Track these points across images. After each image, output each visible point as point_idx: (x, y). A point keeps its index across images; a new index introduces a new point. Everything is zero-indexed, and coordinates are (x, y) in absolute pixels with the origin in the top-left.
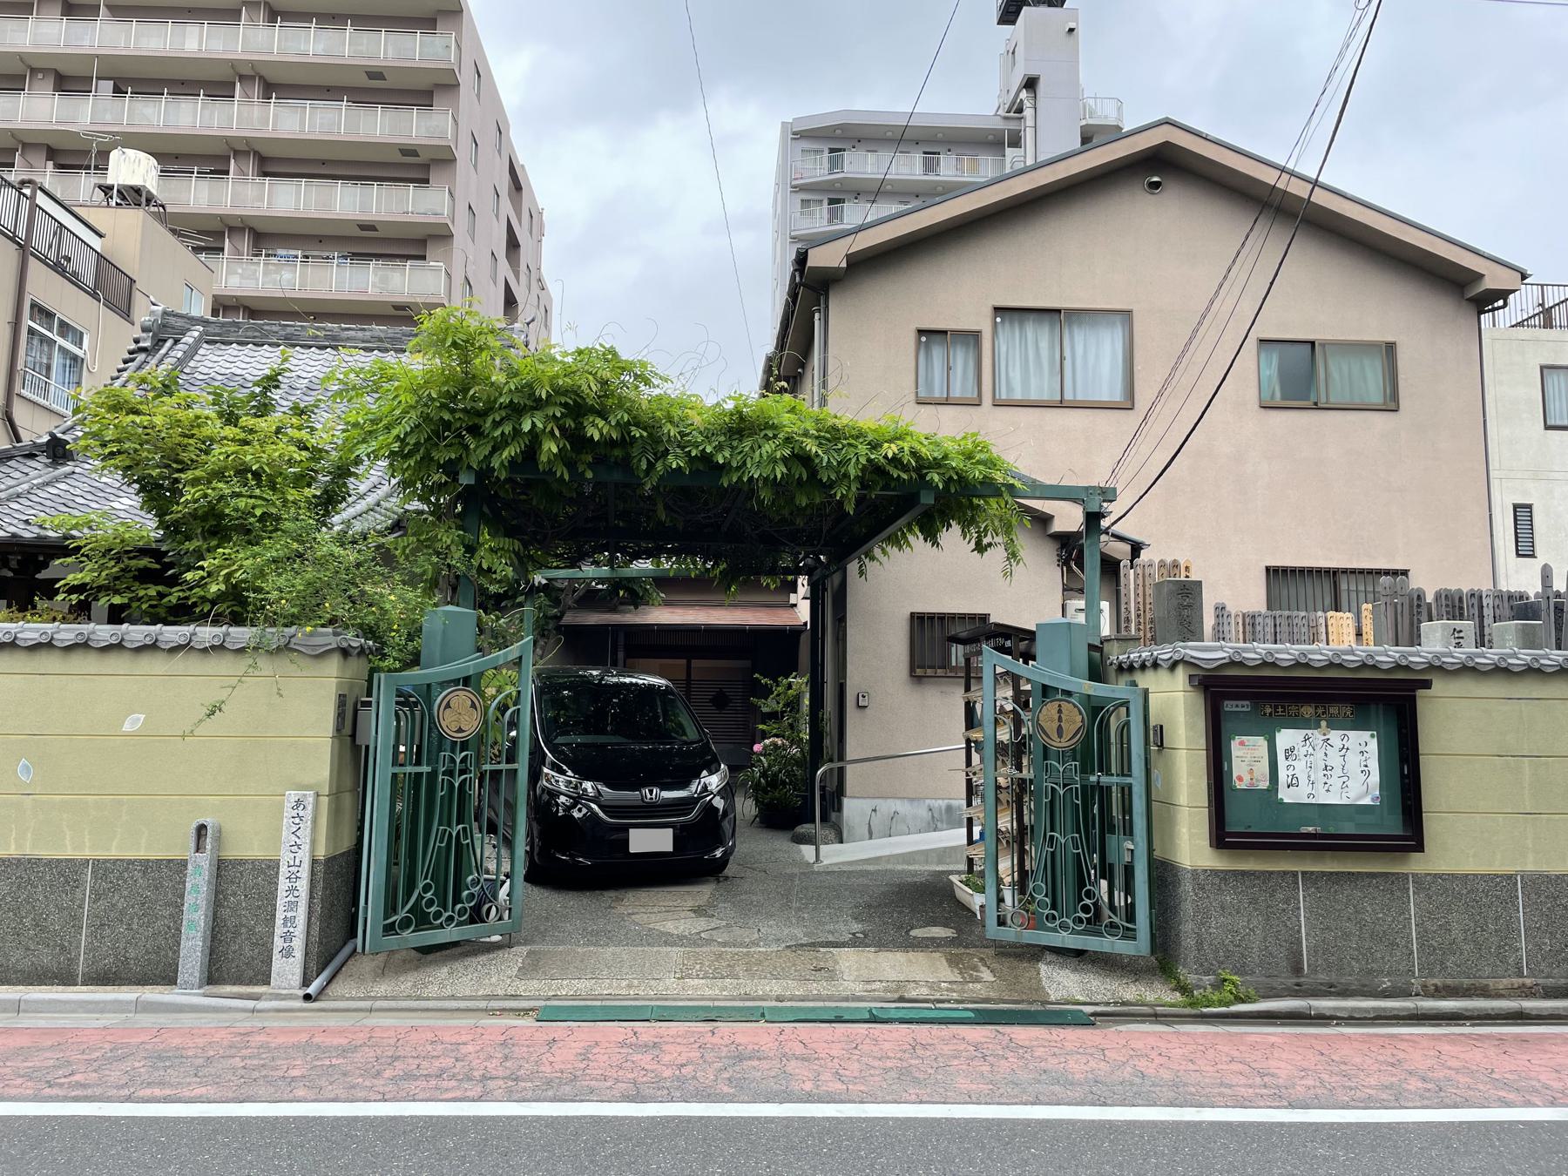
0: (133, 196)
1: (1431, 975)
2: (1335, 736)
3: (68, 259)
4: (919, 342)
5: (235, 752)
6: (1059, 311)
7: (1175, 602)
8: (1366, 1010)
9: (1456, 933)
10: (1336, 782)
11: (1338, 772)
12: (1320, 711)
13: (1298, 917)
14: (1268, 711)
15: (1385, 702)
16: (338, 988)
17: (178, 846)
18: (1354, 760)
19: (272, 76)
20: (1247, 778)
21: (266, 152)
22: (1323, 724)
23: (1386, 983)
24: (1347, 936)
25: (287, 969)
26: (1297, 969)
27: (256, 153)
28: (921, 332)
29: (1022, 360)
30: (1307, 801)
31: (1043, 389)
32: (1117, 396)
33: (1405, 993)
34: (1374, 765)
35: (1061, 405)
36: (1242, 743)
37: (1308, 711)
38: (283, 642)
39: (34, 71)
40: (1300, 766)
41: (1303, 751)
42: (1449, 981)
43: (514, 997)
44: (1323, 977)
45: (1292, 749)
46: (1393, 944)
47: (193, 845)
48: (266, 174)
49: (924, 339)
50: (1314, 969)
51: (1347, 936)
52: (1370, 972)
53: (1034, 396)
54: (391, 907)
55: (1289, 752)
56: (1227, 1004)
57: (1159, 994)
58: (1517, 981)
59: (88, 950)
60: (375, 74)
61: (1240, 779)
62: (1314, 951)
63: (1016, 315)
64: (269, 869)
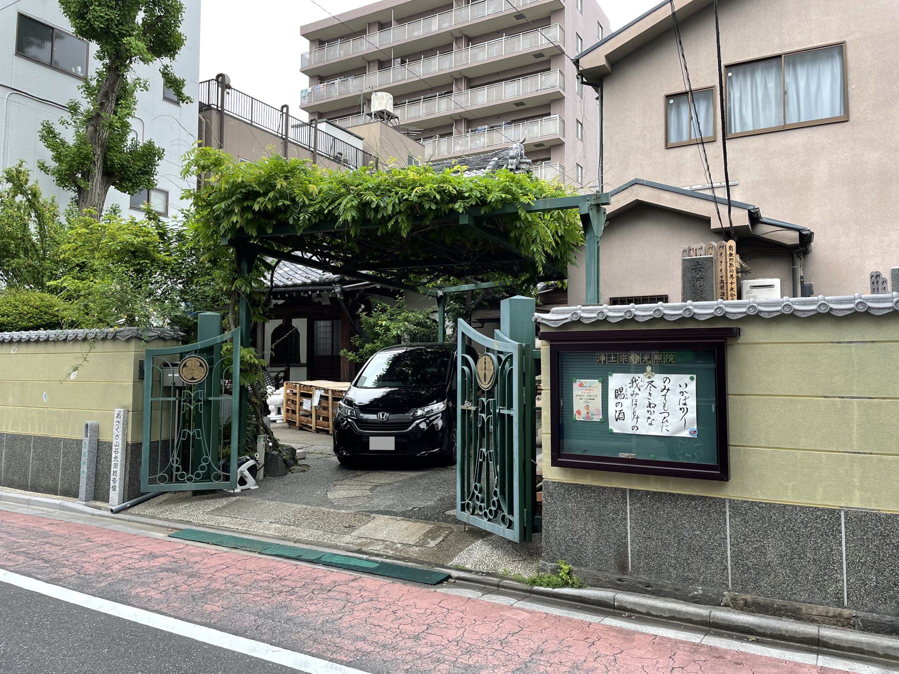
0: (383, 115)
1: (744, 590)
2: (658, 379)
3: (341, 154)
4: (667, 106)
5: (82, 390)
6: (780, 56)
7: (690, 276)
8: (661, 610)
9: (771, 556)
10: (657, 417)
11: (660, 408)
12: (646, 358)
13: (625, 526)
14: (603, 358)
15: (702, 349)
16: (135, 510)
17: (77, 433)
18: (674, 399)
19: (471, 34)
20: (584, 412)
21: (470, 76)
22: (649, 369)
23: (699, 590)
24: (666, 546)
25: (115, 496)
26: (623, 568)
27: (465, 77)
28: (668, 97)
29: (751, 102)
30: (631, 432)
31: (770, 119)
32: (838, 113)
33: (715, 603)
34: (692, 403)
35: (785, 129)
36: (581, 385)
37: (634, 358)
38: (104, 336)
39: (369, 62)
40: (627, 403)
41: (630, 391)
42: (761, 599)
43: (188, 522)
44: (644, 577)
45: (621, 390)
46: (708, 558)
47: (84, 433)
48: (471, 88)
49: (671, 101)
50: (637, 570)
51: (666, 546)
52: (686, 579)
53: (762, 126)
54: (153, 471)
55: (619, 392)
56: (555, 586)
57: (520, 570)
58: (833, 610)
59: (62, 479)
60: (519, 16)
61: (579, 412)
62: (638, 555)
63: (748, 66)
64: (110, 445)
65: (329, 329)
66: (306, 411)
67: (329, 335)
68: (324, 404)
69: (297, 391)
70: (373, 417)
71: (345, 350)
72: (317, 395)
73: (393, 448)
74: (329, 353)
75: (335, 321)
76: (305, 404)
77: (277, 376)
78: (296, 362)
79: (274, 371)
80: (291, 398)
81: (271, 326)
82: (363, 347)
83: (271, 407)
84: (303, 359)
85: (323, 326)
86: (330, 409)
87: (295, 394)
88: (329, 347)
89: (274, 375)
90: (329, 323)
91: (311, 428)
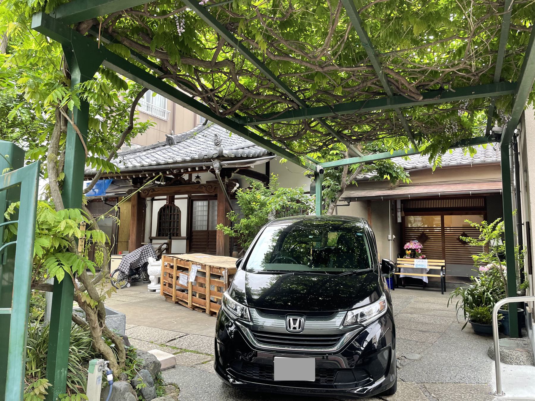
65: (206, 208)
66: (182, 285)
67: (206, 213)
68: (201, 281)
69: (174, 264)
70: (269, 323)
71: (221, 225)
72: (194, 270)
73: (313, 379)
74: (205, 228)
75: (211, 202)
76: (181, 278)
77: (160, 248)
78: (176, 234)
79: (158, 243)
80: (169, 271)
81: (158, 205)
82: (238, 222)
83: (151, 278)
84: (184, 231)
85: (200, 206)
86: (207, 285)
87: (172, 267)
88: (205, 223)
89: (158, 246)
90: (205, 203)
91: (187, 303)
